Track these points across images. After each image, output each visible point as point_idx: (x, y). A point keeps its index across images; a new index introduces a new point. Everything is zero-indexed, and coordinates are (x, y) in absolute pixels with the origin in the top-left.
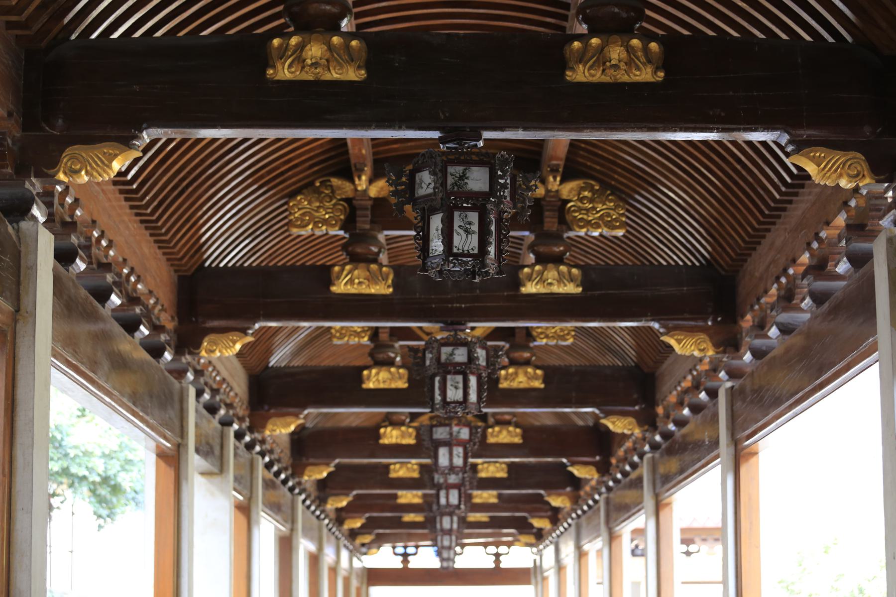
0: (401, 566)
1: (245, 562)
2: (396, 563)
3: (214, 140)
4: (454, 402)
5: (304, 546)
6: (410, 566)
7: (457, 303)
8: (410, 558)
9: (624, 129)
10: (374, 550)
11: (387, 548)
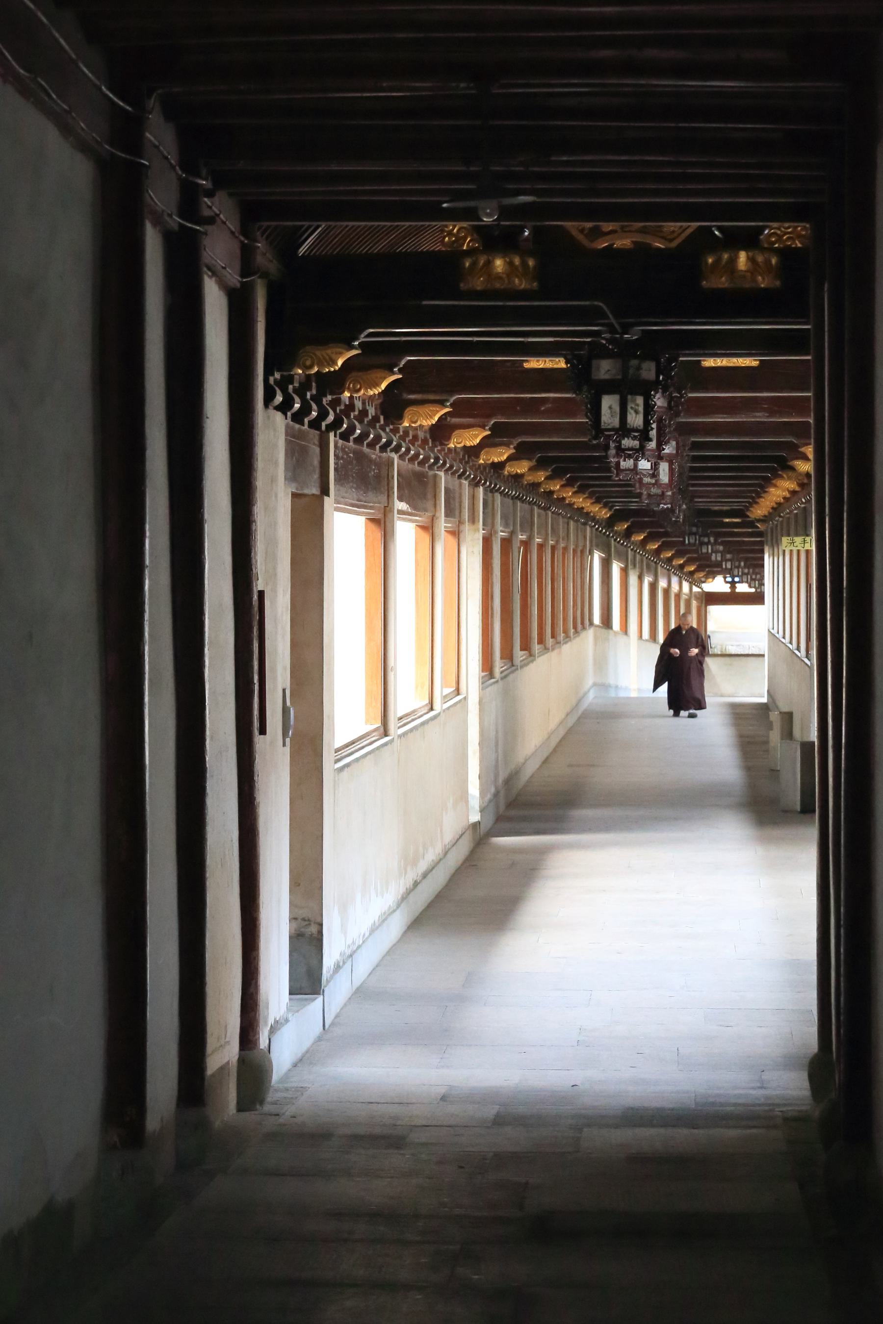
0: (729, 590)
1: (741, 658)
2: (726, 588)
3: (359, 226)
4: (626, 470)
5: (662, 583)
6: (737, 590)
7: (293, 734)
8: (737, 585)
9: (713, 80)
10: (710, 580)
11: (719, 579)
